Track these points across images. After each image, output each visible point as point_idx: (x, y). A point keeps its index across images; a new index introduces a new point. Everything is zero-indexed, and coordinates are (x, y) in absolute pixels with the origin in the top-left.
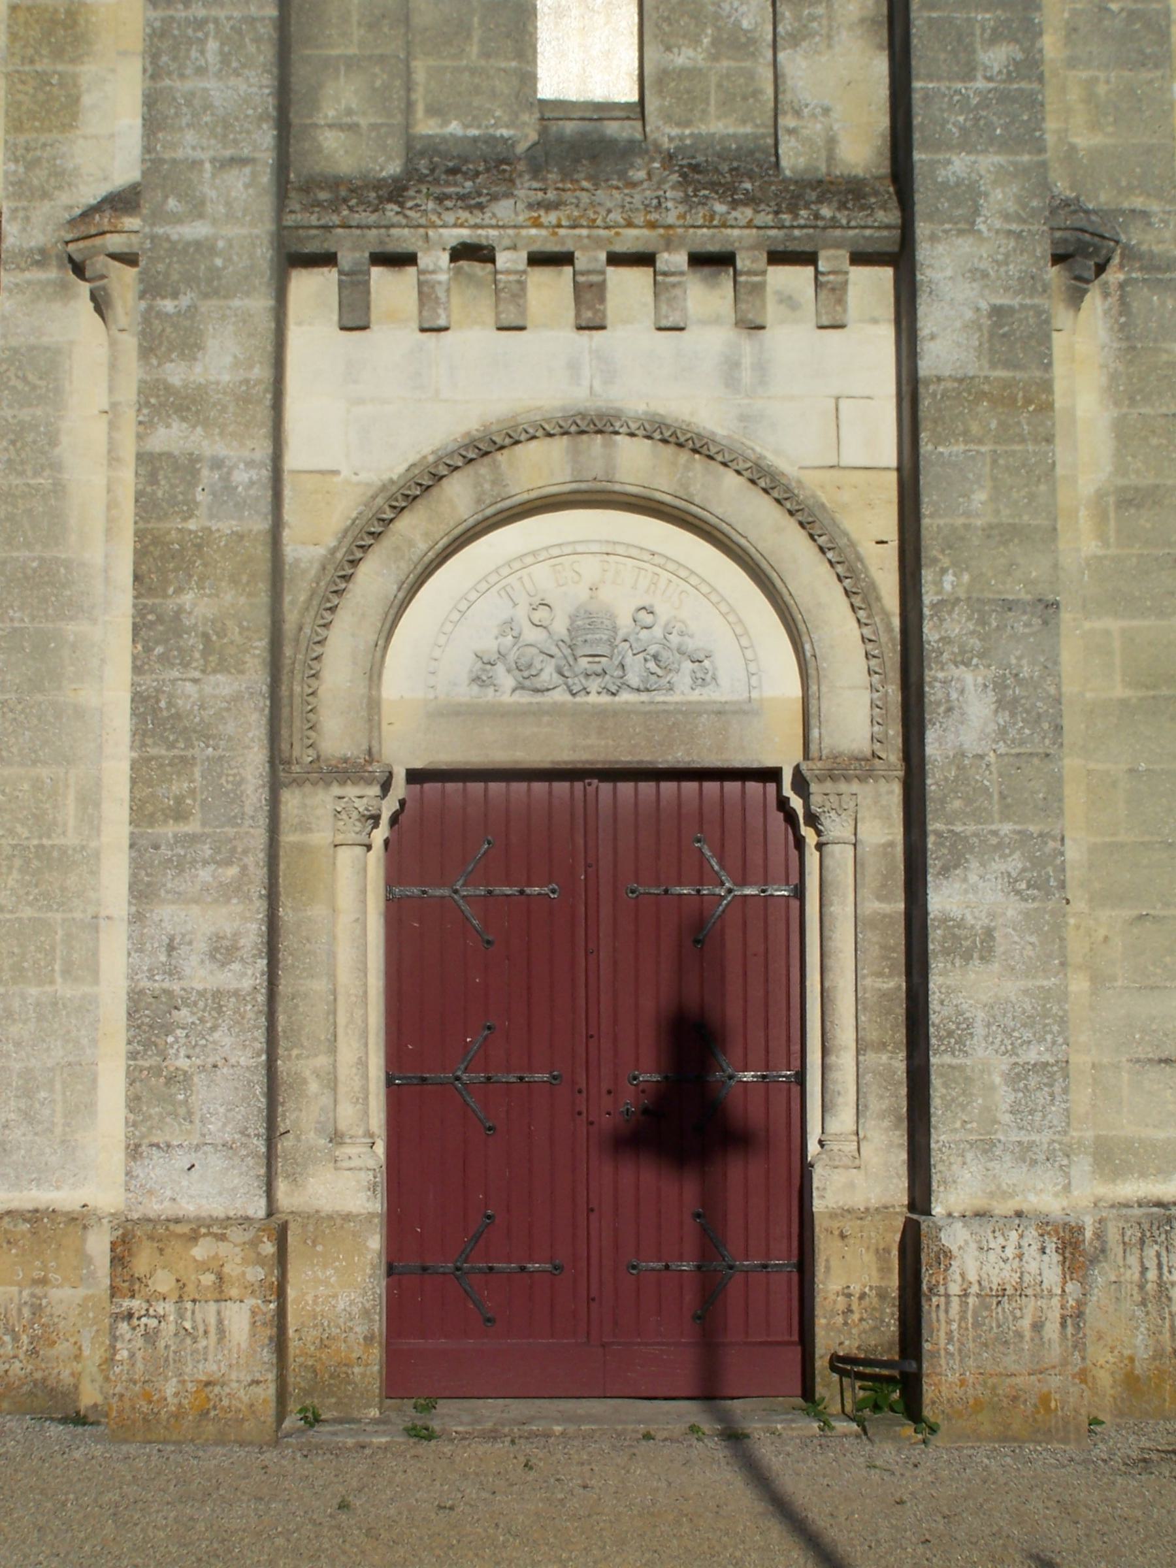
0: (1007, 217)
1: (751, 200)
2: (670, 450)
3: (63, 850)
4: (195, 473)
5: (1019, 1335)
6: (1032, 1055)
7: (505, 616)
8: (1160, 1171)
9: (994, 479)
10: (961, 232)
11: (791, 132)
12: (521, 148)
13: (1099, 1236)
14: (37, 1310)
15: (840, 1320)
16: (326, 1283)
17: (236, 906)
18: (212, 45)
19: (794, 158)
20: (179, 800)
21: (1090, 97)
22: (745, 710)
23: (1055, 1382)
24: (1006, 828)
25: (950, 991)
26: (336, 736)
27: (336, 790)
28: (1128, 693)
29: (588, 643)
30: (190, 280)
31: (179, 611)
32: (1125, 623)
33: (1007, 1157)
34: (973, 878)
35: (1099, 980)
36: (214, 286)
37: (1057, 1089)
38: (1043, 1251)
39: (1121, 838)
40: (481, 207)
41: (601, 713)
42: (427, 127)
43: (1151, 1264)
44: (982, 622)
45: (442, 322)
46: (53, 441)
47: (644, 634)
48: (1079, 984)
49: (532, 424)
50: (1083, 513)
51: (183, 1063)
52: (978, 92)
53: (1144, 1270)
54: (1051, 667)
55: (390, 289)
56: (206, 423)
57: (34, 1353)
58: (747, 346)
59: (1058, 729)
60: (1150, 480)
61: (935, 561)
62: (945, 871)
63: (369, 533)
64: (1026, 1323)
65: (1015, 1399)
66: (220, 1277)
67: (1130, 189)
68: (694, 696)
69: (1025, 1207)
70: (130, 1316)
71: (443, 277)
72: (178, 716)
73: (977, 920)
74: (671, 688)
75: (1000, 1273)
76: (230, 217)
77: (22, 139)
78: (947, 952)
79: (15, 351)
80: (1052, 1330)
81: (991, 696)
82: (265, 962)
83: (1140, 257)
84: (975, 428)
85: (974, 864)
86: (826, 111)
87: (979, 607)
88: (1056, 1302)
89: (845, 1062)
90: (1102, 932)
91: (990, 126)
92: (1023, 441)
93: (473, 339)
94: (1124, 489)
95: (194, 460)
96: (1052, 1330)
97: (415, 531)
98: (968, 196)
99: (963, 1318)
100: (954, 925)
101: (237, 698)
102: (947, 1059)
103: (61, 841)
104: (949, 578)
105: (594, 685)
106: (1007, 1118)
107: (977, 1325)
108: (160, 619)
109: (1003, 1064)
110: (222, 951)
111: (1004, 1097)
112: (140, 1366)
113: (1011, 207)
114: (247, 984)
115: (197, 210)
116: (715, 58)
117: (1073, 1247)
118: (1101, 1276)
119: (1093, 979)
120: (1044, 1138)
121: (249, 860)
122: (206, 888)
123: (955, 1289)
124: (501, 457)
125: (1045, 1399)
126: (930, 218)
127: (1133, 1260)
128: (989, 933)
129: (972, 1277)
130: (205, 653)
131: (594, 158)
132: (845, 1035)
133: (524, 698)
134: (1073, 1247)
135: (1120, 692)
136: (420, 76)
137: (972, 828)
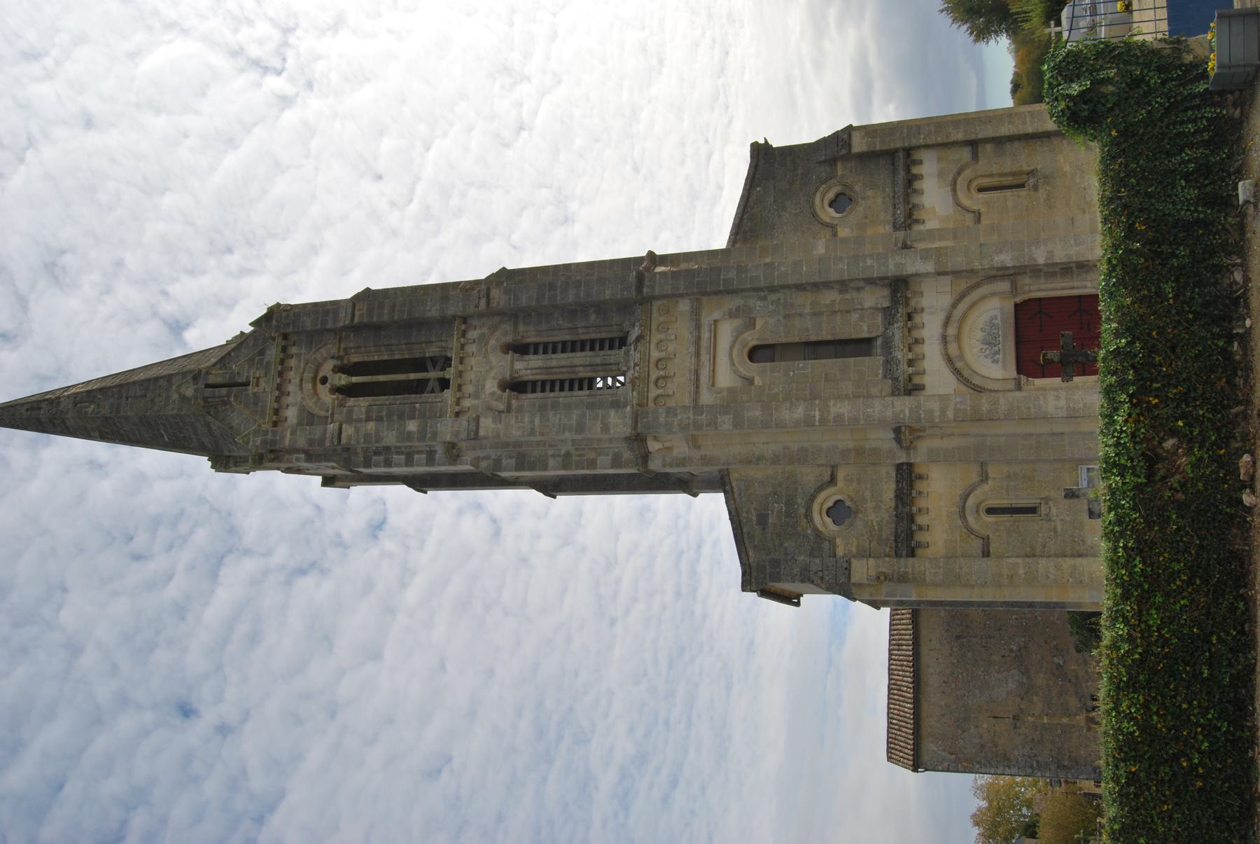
19: (886, 304)
29: (990, 342)
42: (880, 376)
58: (927, 310)
82: (1010, 264)
89: (1075, 284)
93: (926, 364)
97: (966, 373)
98: (897, 265)
110: (1058, 398)
115: (903, 411)
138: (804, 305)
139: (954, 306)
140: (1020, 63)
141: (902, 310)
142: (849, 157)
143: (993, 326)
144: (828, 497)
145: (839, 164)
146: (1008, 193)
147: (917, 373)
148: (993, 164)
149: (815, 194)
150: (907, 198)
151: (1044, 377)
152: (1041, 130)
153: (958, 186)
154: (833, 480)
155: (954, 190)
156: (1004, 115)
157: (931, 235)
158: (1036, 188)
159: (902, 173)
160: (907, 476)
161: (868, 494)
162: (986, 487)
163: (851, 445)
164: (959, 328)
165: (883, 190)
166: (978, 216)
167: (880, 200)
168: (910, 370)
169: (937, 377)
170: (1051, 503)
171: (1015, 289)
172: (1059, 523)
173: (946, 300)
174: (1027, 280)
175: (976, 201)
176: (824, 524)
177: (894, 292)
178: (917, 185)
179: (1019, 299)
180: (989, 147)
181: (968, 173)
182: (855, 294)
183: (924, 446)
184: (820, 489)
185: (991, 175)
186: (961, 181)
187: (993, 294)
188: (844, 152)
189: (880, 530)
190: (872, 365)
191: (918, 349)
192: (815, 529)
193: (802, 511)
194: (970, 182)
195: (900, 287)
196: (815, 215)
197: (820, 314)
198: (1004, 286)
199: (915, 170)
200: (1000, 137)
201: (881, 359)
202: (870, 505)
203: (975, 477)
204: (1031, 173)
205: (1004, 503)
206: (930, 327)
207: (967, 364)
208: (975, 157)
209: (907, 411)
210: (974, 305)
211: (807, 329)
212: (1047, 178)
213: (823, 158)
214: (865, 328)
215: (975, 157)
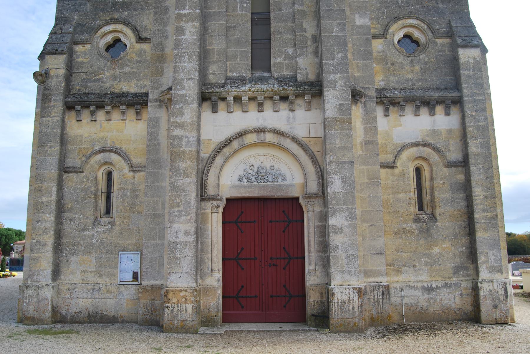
0: (342, 86)
1: (291, 86)
2: (276, 135)
3: (159, 214)
4: (182, 139)
5: (349, 310)
6: (351, 253)
7: (245, 168)
8: (377, 276)
9: (340, 137)
10: (333, 89)
11: (299, 73)
12: (247, 78)
13: (365, 289)
14: (152, 305)
15: (313, 307)
16: (209, 300)
17: (189, 224)
18: (186, 57)
19: (300, 78)
20: (178, 203)
21: (357, 66)
22: (292, 185)
23: (357, 320)
24: (344, 207)
25: (334, 240)
26: (211, 191)
27: (211, 202)
28: (368, 181)
29: (260, 174)
30: (181, 101)
31: (179, 166)
32: (367, 167)
33: (346, 274)
34: (338, 217)
35: (364, 238)
36: (186, 103)
37: (356, 260)
38: (354, 293)
39: (368, 209)
40: (239, 88)
41: (264, 186)
42: (230, 74)
43: (376, 295)
44: (339, 166)
45: (232, 111)
46: (158, 135)
47: (272, 171)
48: (360, 238)
49: (250, 130)
50: (358, 146)
51: (179, 256)
52: (336, 62)
53: (374, 296)
54: (353, 175)
55: (221, 105)
56: (184, 129)
57: (152, 314)
58: (291, 114)
59: (354, 187)
60: (371, 139)
61: (329, 154)
62: (332, 216)
63: (218, 151)
64: (351, 308)
65: (349, 324)
66: (186, 299)
67: (366, 83)
68: (282, 183)
69: (350, 284)
70: (168, 307)
71: (232, 102)
72: (178, 187)
73: (339, 225)
74: (277, 181)
75: (345, 298)
76: (189, 89)
77: (153, 78)
78: (333, 232)
79: (151, 118)
80: (356, 309)
81: (341, 180)
83: (368, 96)
84: (336, 127)
85: (338, 214)
86: (306, 69)
87: (338, 163)
88: (357, 303)
89: (313, 254)
90: (364, 228)
91: (338, 69)
92: (346, 130)
93: (238, 114)
94: (366, 141)
95: (182, 136)
96: (356, 309)
97: (227, 151)
98: (334, 82)
99: (338, 307)
100: (334, 227)
101: (190, 183)
102: (333, 254)
103: (158, 212)
104: (332, 157)
105: (262, 181)
106: (346, 266)
107: (340, 308)
108: (175, 167)
109: (345, 255)
110: (187, 233)
111: (345, 261)
112: (170, 317)
113: (343, 84)
114: (192, 240)
115: (183, 88)
116: (285, 60)
117: (360, 292)
118: (366, 297)
119: (363, 238)
120: (353, 270)
121: (192, 215)
122: (184, 221)
123: (336, 301)
124: (244, 137)
125: (355, 324)
126: (327, 87)
127: (372, 294)
128: (341, 228)
129: (339, 298)
130: (184, 174)
131: (261, 80)
132: (313, 250)
133: (249, 184)
134: (360, 292)
135: (366, 180)
136: (228, 65)
137: (337, 207)
138: (302, 5)
139: (295, 140)
140: (521, 237)
141: (290, 90)
142: (454, 47)
143: (276, 177)
144: (128, 37)
145: (447, 41)
146: (413, 194)
147: (228, 106)
148: (443, 183)
149: (417, 19)
150: (410, 100)
151: (224, 223)
152: (477, 226)
153: (421, 148)
154: (141, 39)
155: (417, 144)
156: (496, 220)
157: (370, 121)
158: (417, 220)
159: (436, 95)
160: (137, 102)
161: (127, 69)
162: (126, 170)
163: (167, 51)
164: (272, 145)
165: (420, 80)
166: (391, 166)
167: (410, 76)
168: (231, 99)
169: (219, 125)
170: (109, 226)
171: (309, 196)
172: (91, 233)
173: (301, 133)
174: (317, 209)
175: (406, 164)
176: (105, 35)
177: (311, 84)
178: (424, 111)
179: (301, 201)
180: (461, 177)
181: (434, 157)
182: (311, 50)
183: (162, 114)
184: (135, 30)
185: (432, 179)
186: (426, 151)
187: (305, 177)
188: (459, 41)
189: (94, 81)
190: (242, 66)
191: (253, 106)
192: (100, 27)
193: (117, 16)
194: (426, 159)
195: (315, 90)
196: (397, 19)
197: (294, 20)
198: (313, 187)
199: (439, 109)
200: (471, 187)
201: (248, 74)
202: (118, 71)
203: (136, 160)
204: (433, 217)
205: (115, 187)
206: (275, 117)
207: (236, 152)
208: (451, 165)
209: (184, 92)
210: (296, 158)
211: (280, 10)
212: (426, 232)
213: (454, 25)
214: (279, 60)
215: (451, 165)
